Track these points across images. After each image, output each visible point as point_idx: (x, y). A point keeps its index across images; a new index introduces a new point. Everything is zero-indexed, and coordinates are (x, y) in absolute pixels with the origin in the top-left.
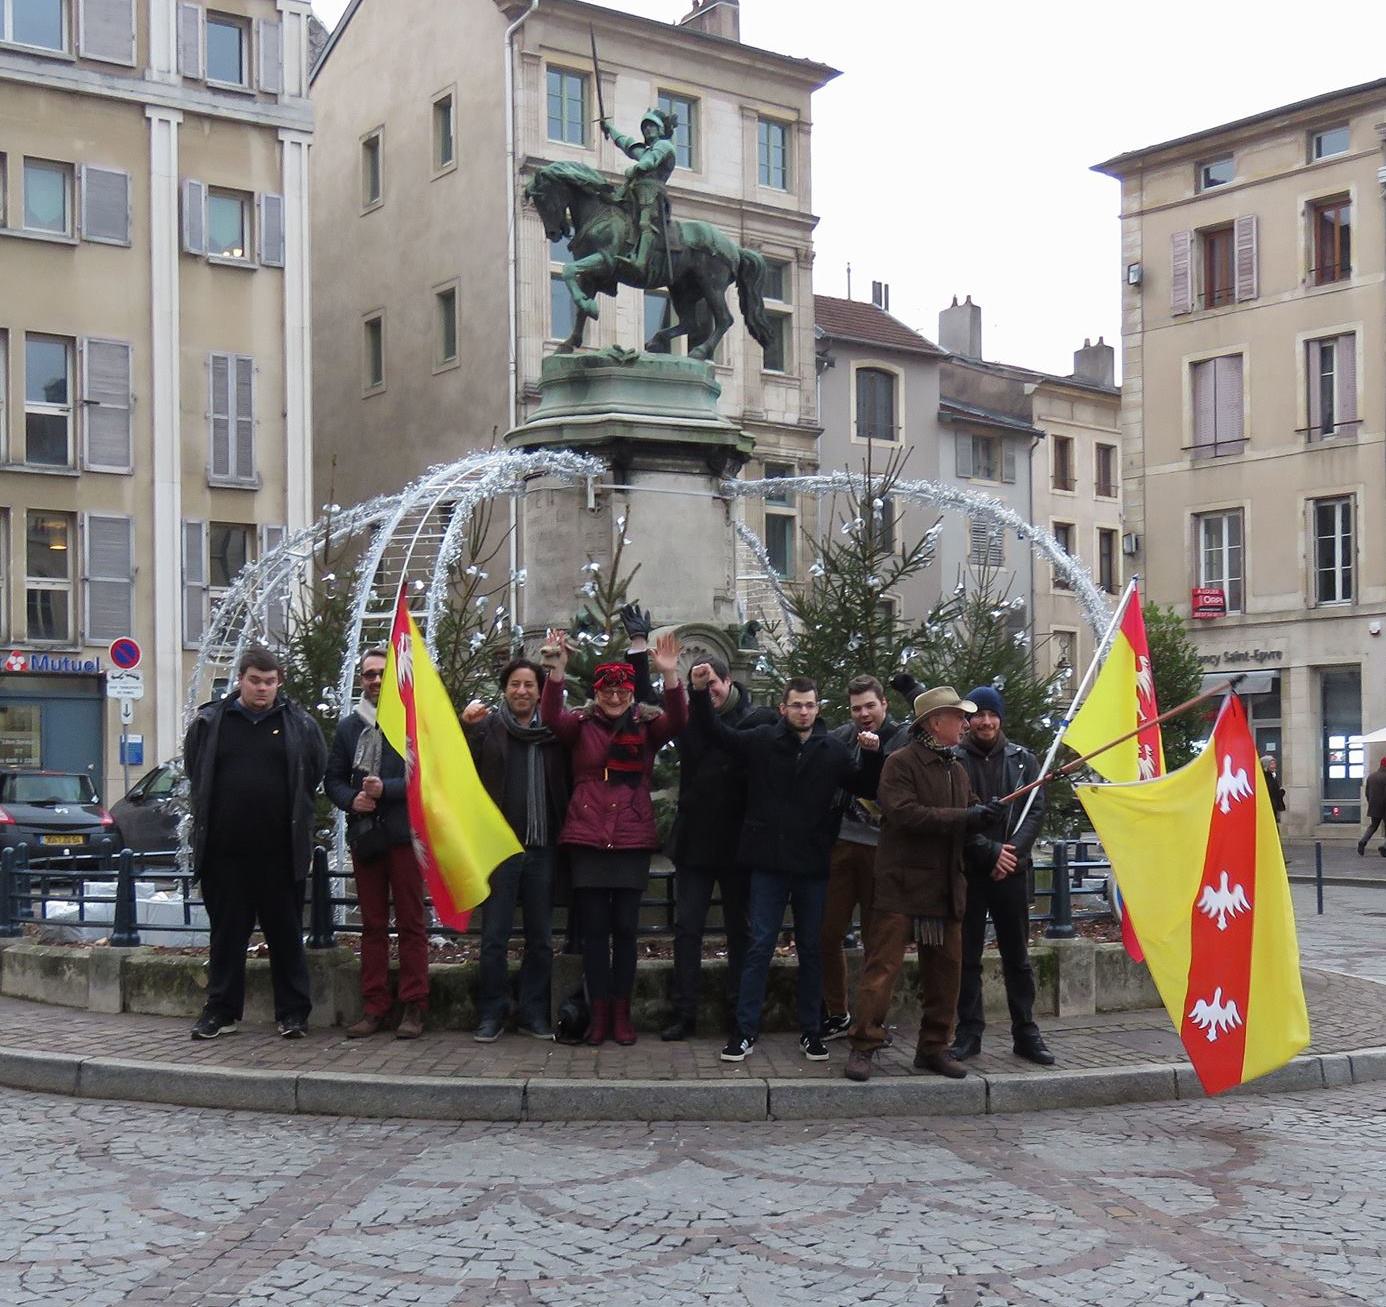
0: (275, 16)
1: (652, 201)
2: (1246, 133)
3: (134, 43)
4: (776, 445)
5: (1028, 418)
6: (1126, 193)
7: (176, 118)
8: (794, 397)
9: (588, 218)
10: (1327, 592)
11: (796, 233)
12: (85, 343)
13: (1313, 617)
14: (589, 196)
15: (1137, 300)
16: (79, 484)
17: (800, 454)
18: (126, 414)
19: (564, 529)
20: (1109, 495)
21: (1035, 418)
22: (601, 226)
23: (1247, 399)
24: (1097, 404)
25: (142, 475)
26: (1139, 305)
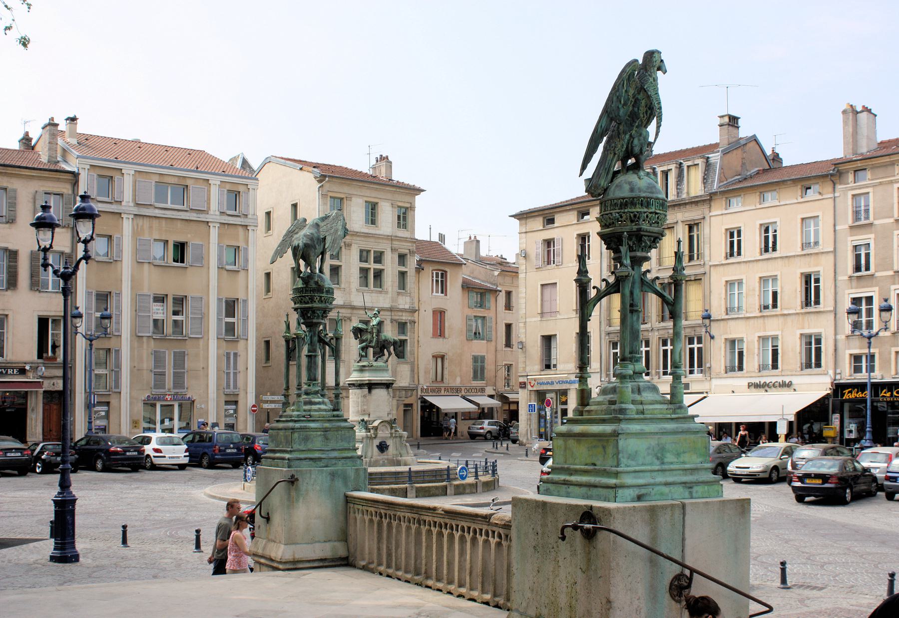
6: (521, 225)
8: (408, 299)
25: (206, 338)
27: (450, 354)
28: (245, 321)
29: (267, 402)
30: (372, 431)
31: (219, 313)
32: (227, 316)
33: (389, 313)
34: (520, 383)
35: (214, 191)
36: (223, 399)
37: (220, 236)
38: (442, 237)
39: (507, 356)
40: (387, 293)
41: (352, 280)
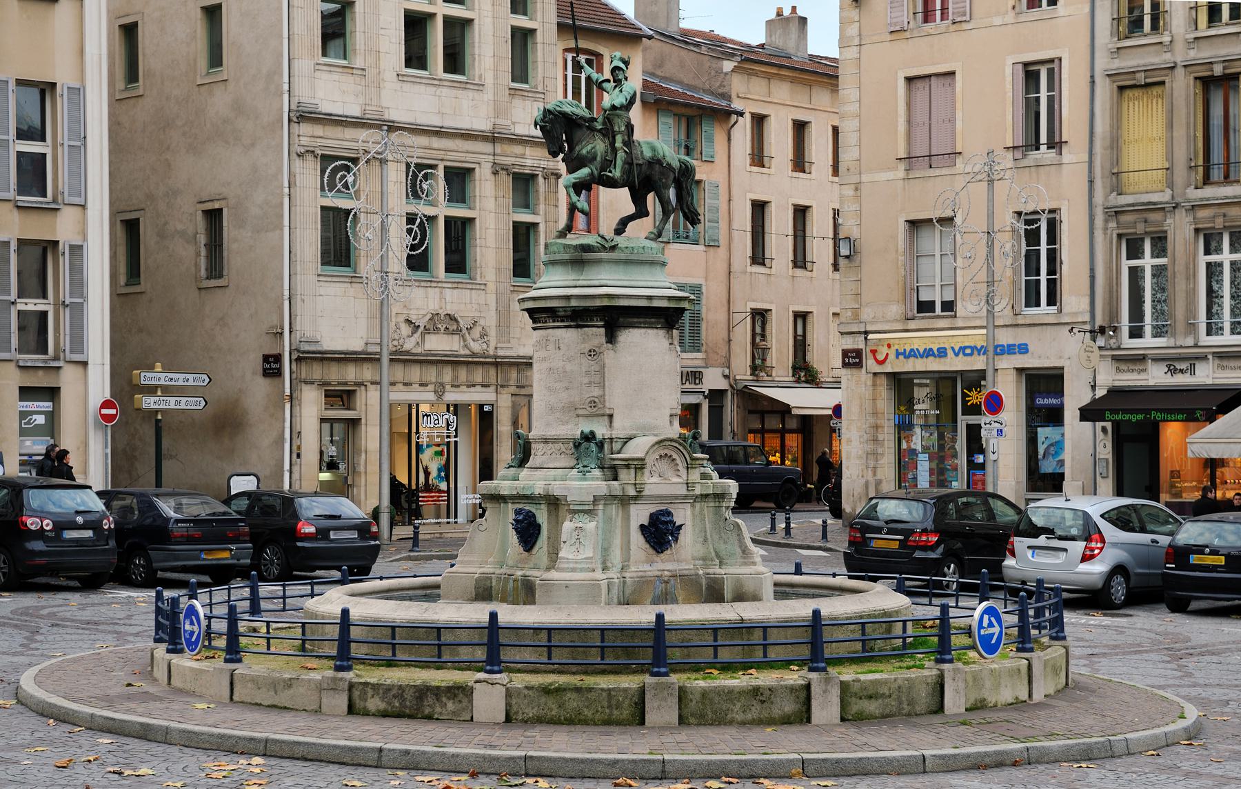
1: (623, 128)
4: (523, 156)
5: (728, 97)
9: (580, 141)
10: (1032, 299)
14: (580, 126)
15: (854, 14)
17: (543, 164)
19: (569, 367)
21: (734, 96)
22: (589, 147)
23: (959, 115)
24: (793, 81)
26: (857, 19)
28: (78, 151)
29: (151, 390)
30: (625, 475)
33: (488, 147)
40: (480, 86)
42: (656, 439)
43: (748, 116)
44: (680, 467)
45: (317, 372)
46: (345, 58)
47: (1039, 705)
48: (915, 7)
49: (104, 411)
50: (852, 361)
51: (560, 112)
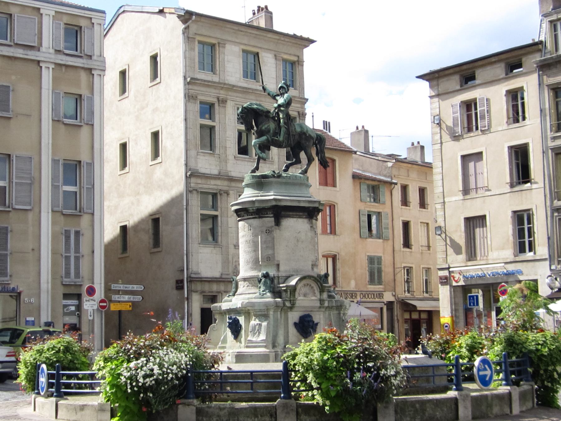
0: (91, 25)
2: (480, 63)
3: (36, 37)
6: (431, 87)
7: (52, 66)
9: (262, 123)
11: (299, 106)
12: (14, 157)
13: (517, 260)
14: (261, 115)
16: (11, 214)
18: (31, 184)
20: (425, 208)
22: (266, 126)
25: (36, 210)
27: (343, 254)
31: (54, 178)
32: (66, 183)
34: (441, 278)
35: (47, 24)
36: (61, 291)
37: (55, 80)
38: (326, 125)
39: (406, 258)
41: (228, 144)
42: (301, 276)
43: (399, 185)
44: (316, 291)
45: (199, 287)
46: (211, 150)
47: (517, 416)
48: (464, 125)
49: (101, 304)
50: (443, 281)
51: (250, 108)
